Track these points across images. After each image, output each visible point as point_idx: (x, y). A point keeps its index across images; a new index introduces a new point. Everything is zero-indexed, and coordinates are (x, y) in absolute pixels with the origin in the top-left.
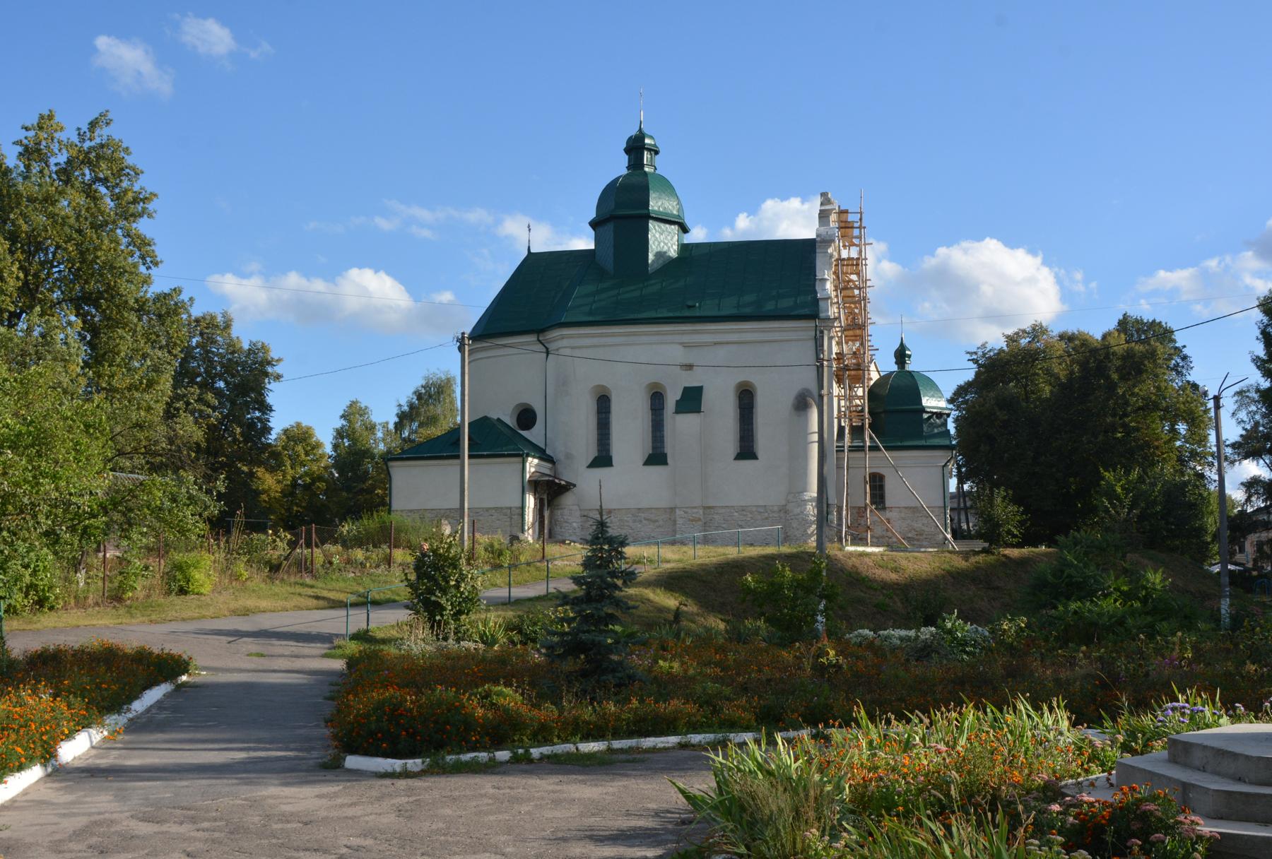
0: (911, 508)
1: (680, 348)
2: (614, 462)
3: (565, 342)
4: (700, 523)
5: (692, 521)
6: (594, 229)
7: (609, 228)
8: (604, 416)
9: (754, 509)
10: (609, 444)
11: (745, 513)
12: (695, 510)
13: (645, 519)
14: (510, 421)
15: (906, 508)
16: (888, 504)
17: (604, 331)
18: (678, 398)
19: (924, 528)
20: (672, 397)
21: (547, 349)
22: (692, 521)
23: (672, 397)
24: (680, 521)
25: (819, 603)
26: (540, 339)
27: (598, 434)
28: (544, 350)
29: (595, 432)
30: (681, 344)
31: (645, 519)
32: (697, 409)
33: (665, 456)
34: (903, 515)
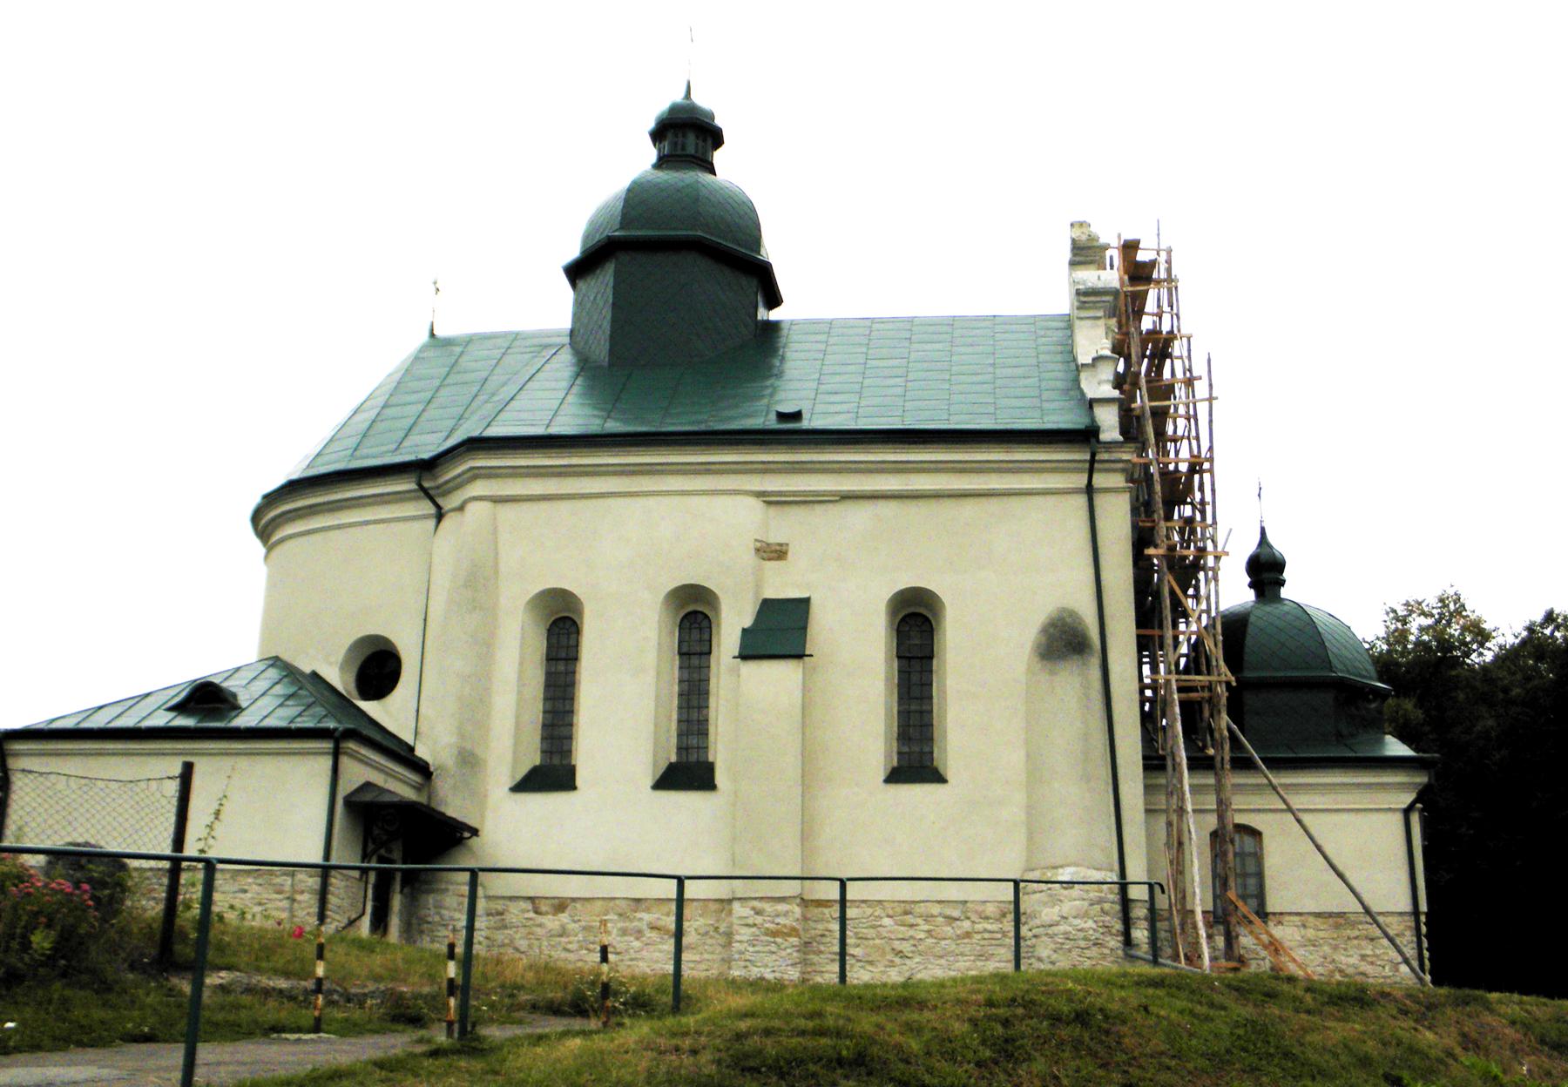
0: (1330, 915)
1: (752, 501)
2: (579, 781)
3: (479, 488)
4: (794, 940)
5: (775, 934)
6: (573, 284)
7: (603, 281)
8: (561, 667)
9: (936, 910)
10: (570, 738)
11: (909, 919)
12: (781, 907)
13: (653, 928)
14: (338, 677)
15: (1318, 915)
16: (1273, 905)
17: (575, 461)
18: (748, 622)
19: (1365, 967)
20: (733, 622)
21: (439, 507)
22: (775, 934)
23: (733, 622)
24: (744, 934)
25: (317, 999)
26: (426, 485)
27: (543, 739)
28: (432, 510)
29: (539, 706)
30: (759, 494)
31: (653, 928)
32: (794, 650)
33: (709, 768)
34: (1311, 933)
